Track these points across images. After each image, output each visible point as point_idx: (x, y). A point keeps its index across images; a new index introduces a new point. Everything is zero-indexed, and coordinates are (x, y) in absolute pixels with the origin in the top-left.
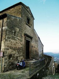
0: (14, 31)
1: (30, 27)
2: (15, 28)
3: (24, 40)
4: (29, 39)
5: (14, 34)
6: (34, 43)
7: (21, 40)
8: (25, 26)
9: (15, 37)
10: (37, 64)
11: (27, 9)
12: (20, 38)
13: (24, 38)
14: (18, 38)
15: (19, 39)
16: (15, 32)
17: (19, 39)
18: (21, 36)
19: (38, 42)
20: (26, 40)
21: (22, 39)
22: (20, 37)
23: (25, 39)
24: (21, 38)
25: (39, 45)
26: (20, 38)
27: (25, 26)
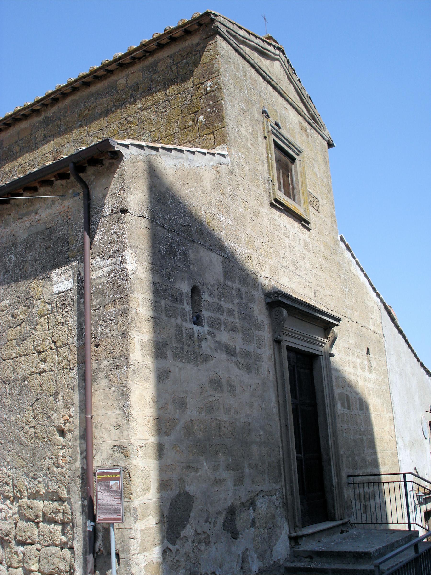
0: (185, 288)
1: (304, 222)
2: (192, 256)
3: (267, 351)
4: (298, 336)
5: (187, 308)
6: (210, 569)
7: (247, 354)
8: (265, 221)
9: (201, 339)
10: (239, 67)
11: (264, 63)
12: (237, 342)
13: (266, 334)
14: (224, 337)
15: (230, 351)
16: (195, 291)
17: (230, 351)
18: (247, 316)
19: (382, 351)
20: (290, 349)
21: (251, 348)
22: (234, 329)
23: (278, 342)
24: (247, 339)
25: (394, 378)
26: (237, 342)
27: (265, 221)
